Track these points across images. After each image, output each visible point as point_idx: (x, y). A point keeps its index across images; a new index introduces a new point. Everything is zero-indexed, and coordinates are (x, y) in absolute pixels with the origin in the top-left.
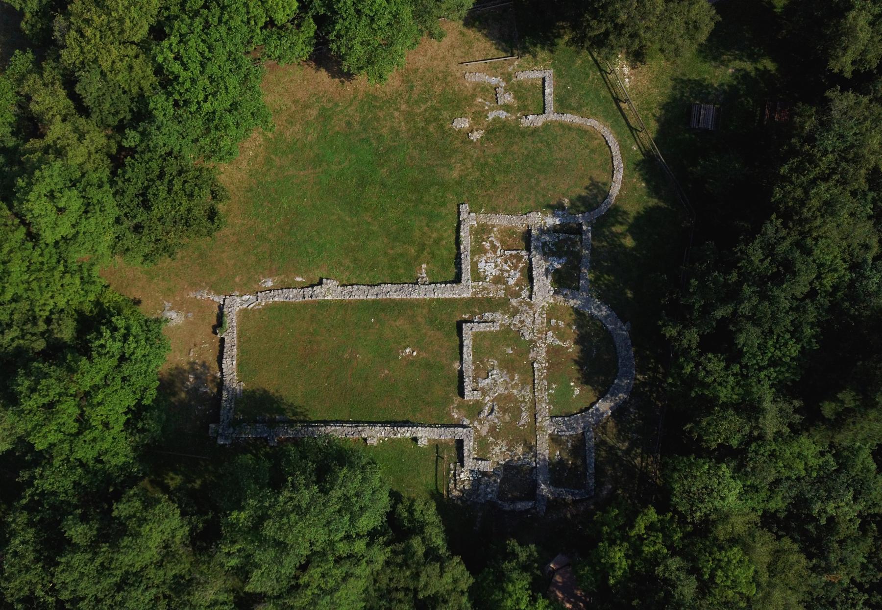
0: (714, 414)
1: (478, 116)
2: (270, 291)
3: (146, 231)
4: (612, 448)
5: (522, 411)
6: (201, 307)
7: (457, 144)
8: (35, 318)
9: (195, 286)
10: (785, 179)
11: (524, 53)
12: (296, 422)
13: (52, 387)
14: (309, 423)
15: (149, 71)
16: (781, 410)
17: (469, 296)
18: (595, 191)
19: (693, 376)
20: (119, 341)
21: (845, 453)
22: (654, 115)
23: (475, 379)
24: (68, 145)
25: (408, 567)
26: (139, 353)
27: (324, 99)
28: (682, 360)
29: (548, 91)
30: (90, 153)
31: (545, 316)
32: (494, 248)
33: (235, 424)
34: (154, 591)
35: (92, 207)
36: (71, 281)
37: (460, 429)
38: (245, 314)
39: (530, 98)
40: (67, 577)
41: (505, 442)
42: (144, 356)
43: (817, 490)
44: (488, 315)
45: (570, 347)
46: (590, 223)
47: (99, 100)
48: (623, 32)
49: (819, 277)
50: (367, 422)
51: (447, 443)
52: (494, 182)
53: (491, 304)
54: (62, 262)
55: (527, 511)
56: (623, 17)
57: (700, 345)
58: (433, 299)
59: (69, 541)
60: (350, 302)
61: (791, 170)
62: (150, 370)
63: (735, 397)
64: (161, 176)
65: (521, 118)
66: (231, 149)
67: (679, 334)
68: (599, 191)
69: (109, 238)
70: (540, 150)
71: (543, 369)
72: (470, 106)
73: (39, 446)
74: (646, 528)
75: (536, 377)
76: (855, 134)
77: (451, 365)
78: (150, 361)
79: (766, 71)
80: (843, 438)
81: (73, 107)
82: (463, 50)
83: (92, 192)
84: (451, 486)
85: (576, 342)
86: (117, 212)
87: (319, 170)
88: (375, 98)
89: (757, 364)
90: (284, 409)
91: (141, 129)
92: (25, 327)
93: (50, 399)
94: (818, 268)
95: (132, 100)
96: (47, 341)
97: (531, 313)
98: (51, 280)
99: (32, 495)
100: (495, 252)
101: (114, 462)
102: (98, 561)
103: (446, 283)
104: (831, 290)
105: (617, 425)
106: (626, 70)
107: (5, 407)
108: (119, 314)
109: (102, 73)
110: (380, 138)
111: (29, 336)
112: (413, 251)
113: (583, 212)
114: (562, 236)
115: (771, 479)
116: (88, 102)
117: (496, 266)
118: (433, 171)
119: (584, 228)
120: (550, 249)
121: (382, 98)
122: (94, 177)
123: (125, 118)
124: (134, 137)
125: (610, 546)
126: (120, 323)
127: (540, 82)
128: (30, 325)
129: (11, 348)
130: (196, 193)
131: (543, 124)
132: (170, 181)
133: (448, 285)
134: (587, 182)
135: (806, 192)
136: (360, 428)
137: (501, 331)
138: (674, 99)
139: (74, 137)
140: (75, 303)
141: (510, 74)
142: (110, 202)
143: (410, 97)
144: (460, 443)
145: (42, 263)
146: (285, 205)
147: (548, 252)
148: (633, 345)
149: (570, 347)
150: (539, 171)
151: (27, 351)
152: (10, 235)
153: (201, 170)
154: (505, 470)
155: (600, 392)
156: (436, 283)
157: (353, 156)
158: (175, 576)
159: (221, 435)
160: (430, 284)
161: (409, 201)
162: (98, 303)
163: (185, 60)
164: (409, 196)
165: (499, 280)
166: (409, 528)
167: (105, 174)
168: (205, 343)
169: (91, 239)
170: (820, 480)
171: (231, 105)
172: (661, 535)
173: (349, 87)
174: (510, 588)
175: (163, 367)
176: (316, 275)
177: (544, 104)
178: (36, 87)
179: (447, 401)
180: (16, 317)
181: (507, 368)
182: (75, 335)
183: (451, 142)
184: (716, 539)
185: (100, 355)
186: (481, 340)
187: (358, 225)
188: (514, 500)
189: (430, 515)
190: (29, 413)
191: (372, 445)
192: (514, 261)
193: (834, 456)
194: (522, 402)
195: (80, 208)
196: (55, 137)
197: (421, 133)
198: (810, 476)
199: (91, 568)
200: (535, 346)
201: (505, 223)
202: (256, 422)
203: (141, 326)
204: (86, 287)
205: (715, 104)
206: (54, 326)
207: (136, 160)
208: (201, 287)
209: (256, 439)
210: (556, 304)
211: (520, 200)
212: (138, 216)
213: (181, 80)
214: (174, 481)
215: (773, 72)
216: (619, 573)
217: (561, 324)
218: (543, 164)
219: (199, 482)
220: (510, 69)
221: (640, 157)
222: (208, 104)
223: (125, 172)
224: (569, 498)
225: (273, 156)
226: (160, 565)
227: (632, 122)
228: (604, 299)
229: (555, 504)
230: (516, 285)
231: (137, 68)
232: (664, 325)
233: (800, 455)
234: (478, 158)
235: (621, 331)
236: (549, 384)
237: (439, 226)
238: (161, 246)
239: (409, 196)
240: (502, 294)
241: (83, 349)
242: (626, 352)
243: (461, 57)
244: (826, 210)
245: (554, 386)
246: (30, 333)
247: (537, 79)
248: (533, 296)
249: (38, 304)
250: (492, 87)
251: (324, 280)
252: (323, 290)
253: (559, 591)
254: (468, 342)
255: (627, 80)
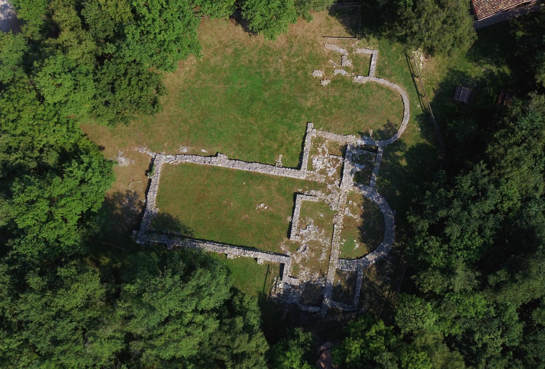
0: (428, 272)
1: (329, 71)
2: (185, 155)
3: (111, 106)
4: (372, 283)
5: (322, 252)
6: (141, 157)
7: (313, 85)
8: (33, 148)
9: (139, 144)
10: (496, 140)
11: (362, 37)
12: (186, 237)
13: (34, 192)
14: (193, 240)
15: (128, 9)
16: (468, 276)
17: (304, 178)
18: (389, 128)
19: (421, 248)
20: (82, 170)
21: (501, 308)
22: (433, 89)
23: (299, 229)
24: (71, 46)
25: (230, 334)
26: (94, 180)
27: (238, 44)
28: (416, 237)
29: (373, 63)
30: (84, 53)
31: (346, 198)
32: (324, 152)
33: (149, 232)
34: (75, 324)
35: (78, 87)
36: (60, 129)
37: (284, 257)
38: (167, 166)
39: (361, 65)
40: (23, 307)
41: (309, 269)
42: (97, 182)
43: (480, 326)
44: (313, 192)
45: (358, 219)
46: (383, 147)
47: (96, 21)
48: (415, 37)
49: (501, 202)
50: (229, 245)
51: (275, 264)
52: (331, 113)
53: (315, 186)
54: (57, 116)
55: (315, 313)
56: (415, 28)
57: (429, 230)
58: (282, 177)
59: (28, 285)
60: (232, 170)
61: (501, 136)
62: (100, 191)
63: (441, 264)
64: (125, 74)
65: (354, 76)
66: (172, 64)
67: (418, 221)
68: (392, 129)
69: (88, 106)
70: (362, 98)
71: (339, 229)
72: (325, 64)
73: (20, 226)
74: (376, 332)
75: (334, 233)
76: (540, 121)
77: (286, 218)
78: (100, 186)
79: (504, 74)
80: (500, 298)
81: (80, 22)
82: (326, 29)
83: (80, 78)
84: (273, 291)
85: (362, 216)
86: (94, 91)
87: (227, 86)
88: (269, 49)
89: (458, 247)
90: (179, 229)
91: (117, 44)
92: (26, 152)
93: (31, 198)
94: (502, 197)
95: (116, 25)
96: (38, 163)
97: (338, 195)
98: (47, 126)
99: (13, 255)
100: (324, 155)
101: (67, 243)
102: (44, 300)
103: (292, 168)
104: (507, 211)
105: (377, 270)
106: (422, 58)
107: (6, 199)
108: (87, 154)
109: (99, 5)
110: (267, 73)
111: (27, 158)
112: (275, 146)
113: (380, 140)
114: (365, 152)
115: (453, 316)
116: (88, 21)
117: (323, 163)
118: (296, 99)
119: (379, 150)
120: (356, 159)
121: (273, 49)
122: (84, 69)
123: (109, 35)
124: (112, 48)
125: (353, 340)
126: (86, 159)
127: (370, 57)
128: (29, 152)
129: (14, 164)
130: (145, 88)
131: (367, 82)
132: (130, 78)
133: (293, 170)
134: (385, 122)
135: (506, 150)
136: (224, 247)
137: (319, 202)
138: (446, 80)
139: (76, 42)
140: (60, 143)
141: (352, 49)
142: (90, 84)
143: (290, 52)
144: (282, 265)
145: (44, 115)
146: (203, 104)
147: (354, 161)
148: (395, 224)
149: (358, 219)
150: (359, 110)
151: (25, 166)
152: (25, 95)
153: (151, 75)
154: (307, 286)
155: (371, 249)
156: (286, 167)
157: (249, 82)
158: (90, 318)
159: (139, 238)
160: (282, 167)
161: (279, 115)
162: (75, 145)
163: (150, 7)
164: (279, 112)
165: (323, 172)
166: (239, 311)
167: (91, 67)
168: (140, 180)
169: (75, 105)
170: (483, 321)
171: (176, 38)
172: (383, 338)
173: (254, 39)
174: (288, 354)
175: (110, 191)
176: (215, 150)
177: (369, 71)
178: (58, 6)
179: (280, 239)
180: (22, 145)
181: (319, 225)
182: (57, 162)
183: (310, 84)
184: (415, 345)
185: (69, 176)
186: (306, 206)
187: (246, 124)
188: (308, 305)
189: (254, 306)
190: (17, 205)
191: (230, 259)
192: (334, 162)
193: (494, 308)
194: (323, 247)
195: (71, 86)
196: (64, 40)
197: (293, 75)
198: (478, 318)
199: (39, 304)
200: (337, 215)
201: (333, 138)
202: (162, 234)
203: (100, 162)
204: (70, 134)
205: (471, 88)
206: (44, 155)
207: (111, 62)
208: (143, 145)
209: (159, 244)
210: (354, 192)
211: (344, 126)
212: (107, 97)
213: (146, 18)
214: (105, 261)
215: (508, 75)
216: (353, 356)
217: (355, 204)
218: (362, 106)
219: (120, 264)
220: (353, 45)
221: (421, 112)
222: (161, 36)
223: (102, 69)
224: (341, 309)
225: (201, 73)
226: (81, 309)
227: (420, 90)
228: (383, 194)
229: (332, 312)
230: (333, 176)
231: (120, 7)
232: (409, 215)
233: (474, 305)
234: (324, 97)
235: (390, 215)
236: (341, 238)
237: (293, 133)
238: (120, 116)
239: (279, 112)
240: (323, 180)
241: (59, 172)
242: (391, 227)
243: (325, 33)
244: (515, 164)
245: (344, 240)
246: (29, 157)
247: (368, 54)
248: (341, 185)
249: (37, 139)
250: (340, 54)
251: (219, 154)
252: (217, 160)
253: (323, 362)
254: (298, 206)
255: (421, 64)
